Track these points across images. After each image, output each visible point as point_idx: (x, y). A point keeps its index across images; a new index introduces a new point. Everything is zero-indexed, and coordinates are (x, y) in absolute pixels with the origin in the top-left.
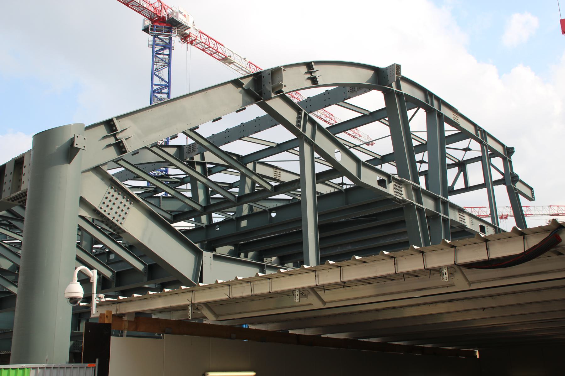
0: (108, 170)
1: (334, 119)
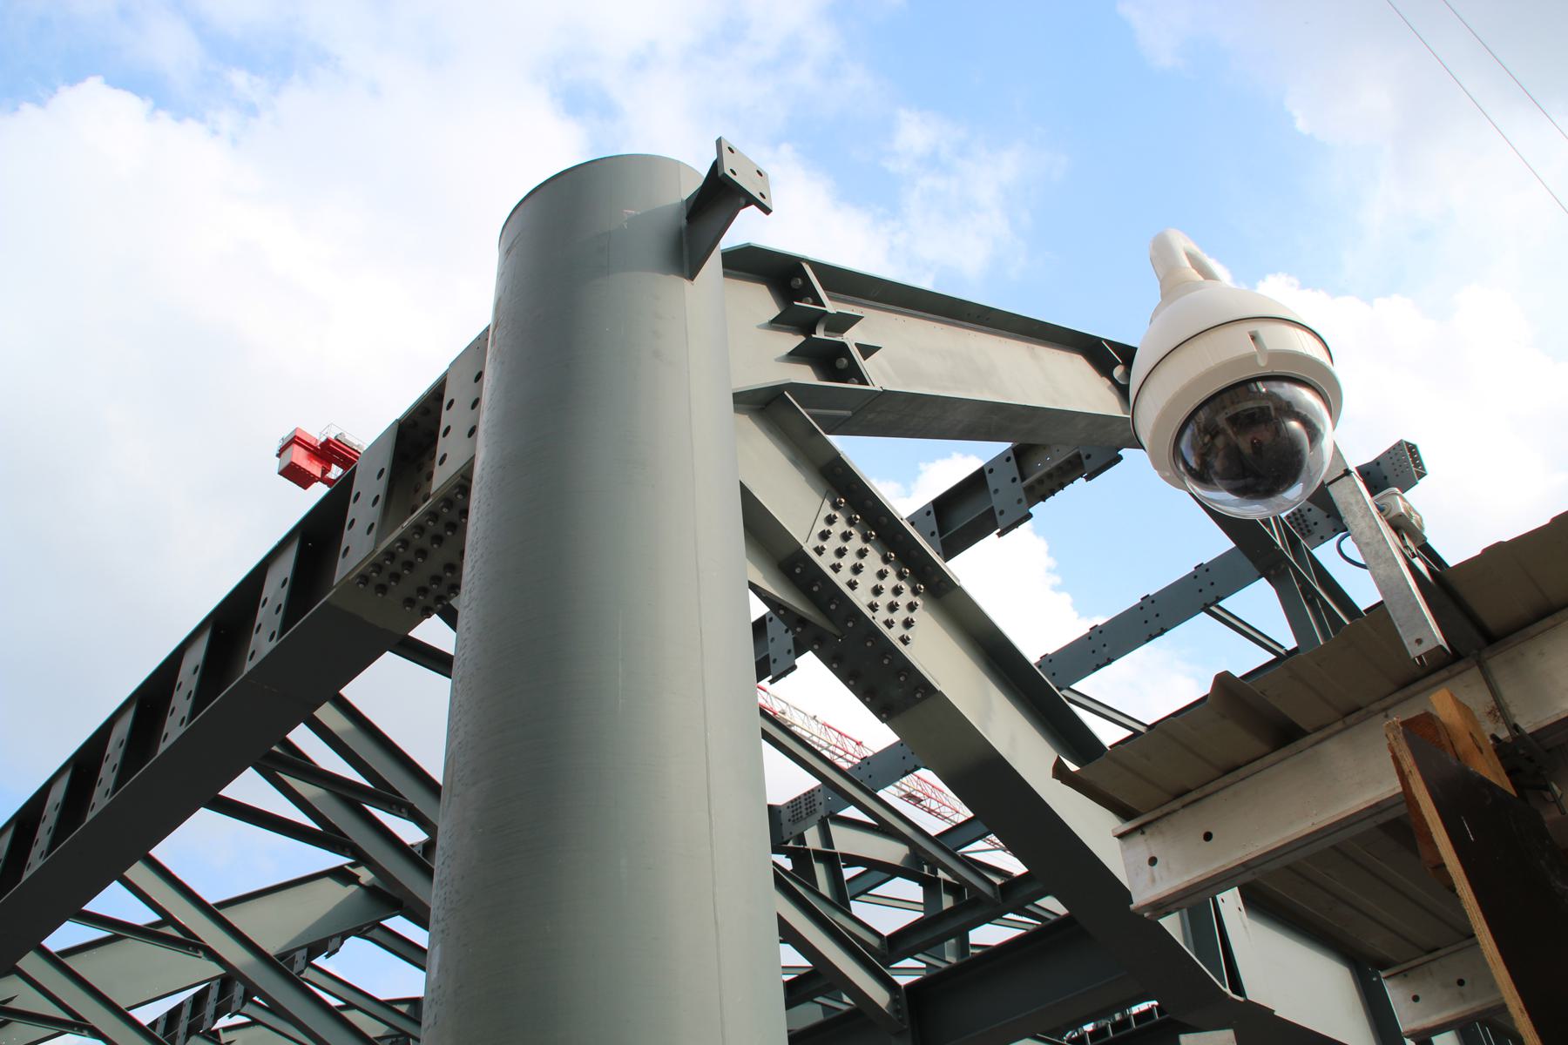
1: (948, 803)
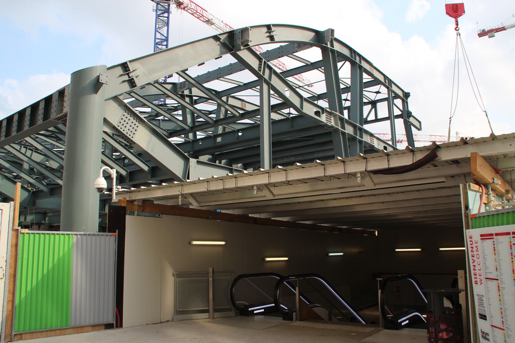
0: (123, 99)
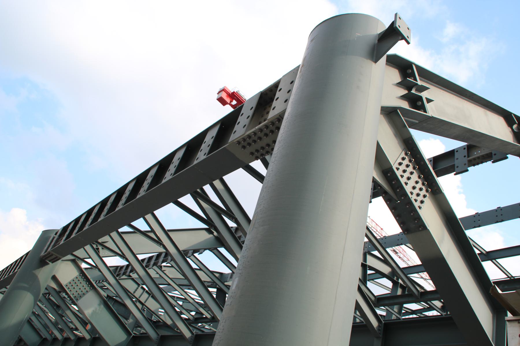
1: (406, 256)
